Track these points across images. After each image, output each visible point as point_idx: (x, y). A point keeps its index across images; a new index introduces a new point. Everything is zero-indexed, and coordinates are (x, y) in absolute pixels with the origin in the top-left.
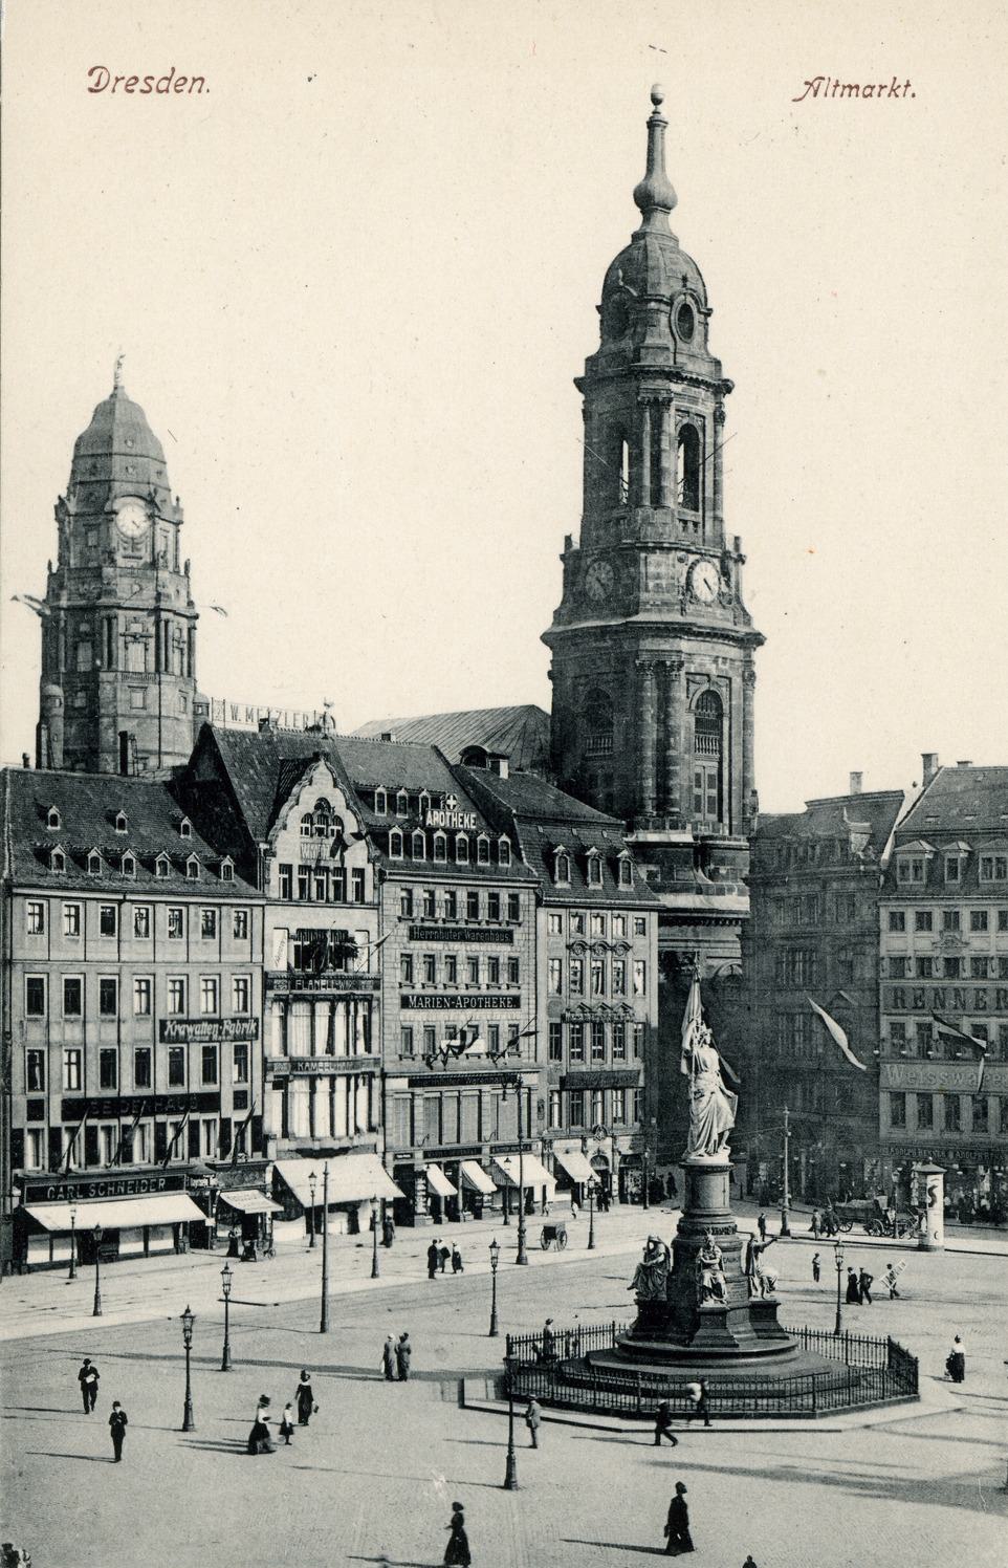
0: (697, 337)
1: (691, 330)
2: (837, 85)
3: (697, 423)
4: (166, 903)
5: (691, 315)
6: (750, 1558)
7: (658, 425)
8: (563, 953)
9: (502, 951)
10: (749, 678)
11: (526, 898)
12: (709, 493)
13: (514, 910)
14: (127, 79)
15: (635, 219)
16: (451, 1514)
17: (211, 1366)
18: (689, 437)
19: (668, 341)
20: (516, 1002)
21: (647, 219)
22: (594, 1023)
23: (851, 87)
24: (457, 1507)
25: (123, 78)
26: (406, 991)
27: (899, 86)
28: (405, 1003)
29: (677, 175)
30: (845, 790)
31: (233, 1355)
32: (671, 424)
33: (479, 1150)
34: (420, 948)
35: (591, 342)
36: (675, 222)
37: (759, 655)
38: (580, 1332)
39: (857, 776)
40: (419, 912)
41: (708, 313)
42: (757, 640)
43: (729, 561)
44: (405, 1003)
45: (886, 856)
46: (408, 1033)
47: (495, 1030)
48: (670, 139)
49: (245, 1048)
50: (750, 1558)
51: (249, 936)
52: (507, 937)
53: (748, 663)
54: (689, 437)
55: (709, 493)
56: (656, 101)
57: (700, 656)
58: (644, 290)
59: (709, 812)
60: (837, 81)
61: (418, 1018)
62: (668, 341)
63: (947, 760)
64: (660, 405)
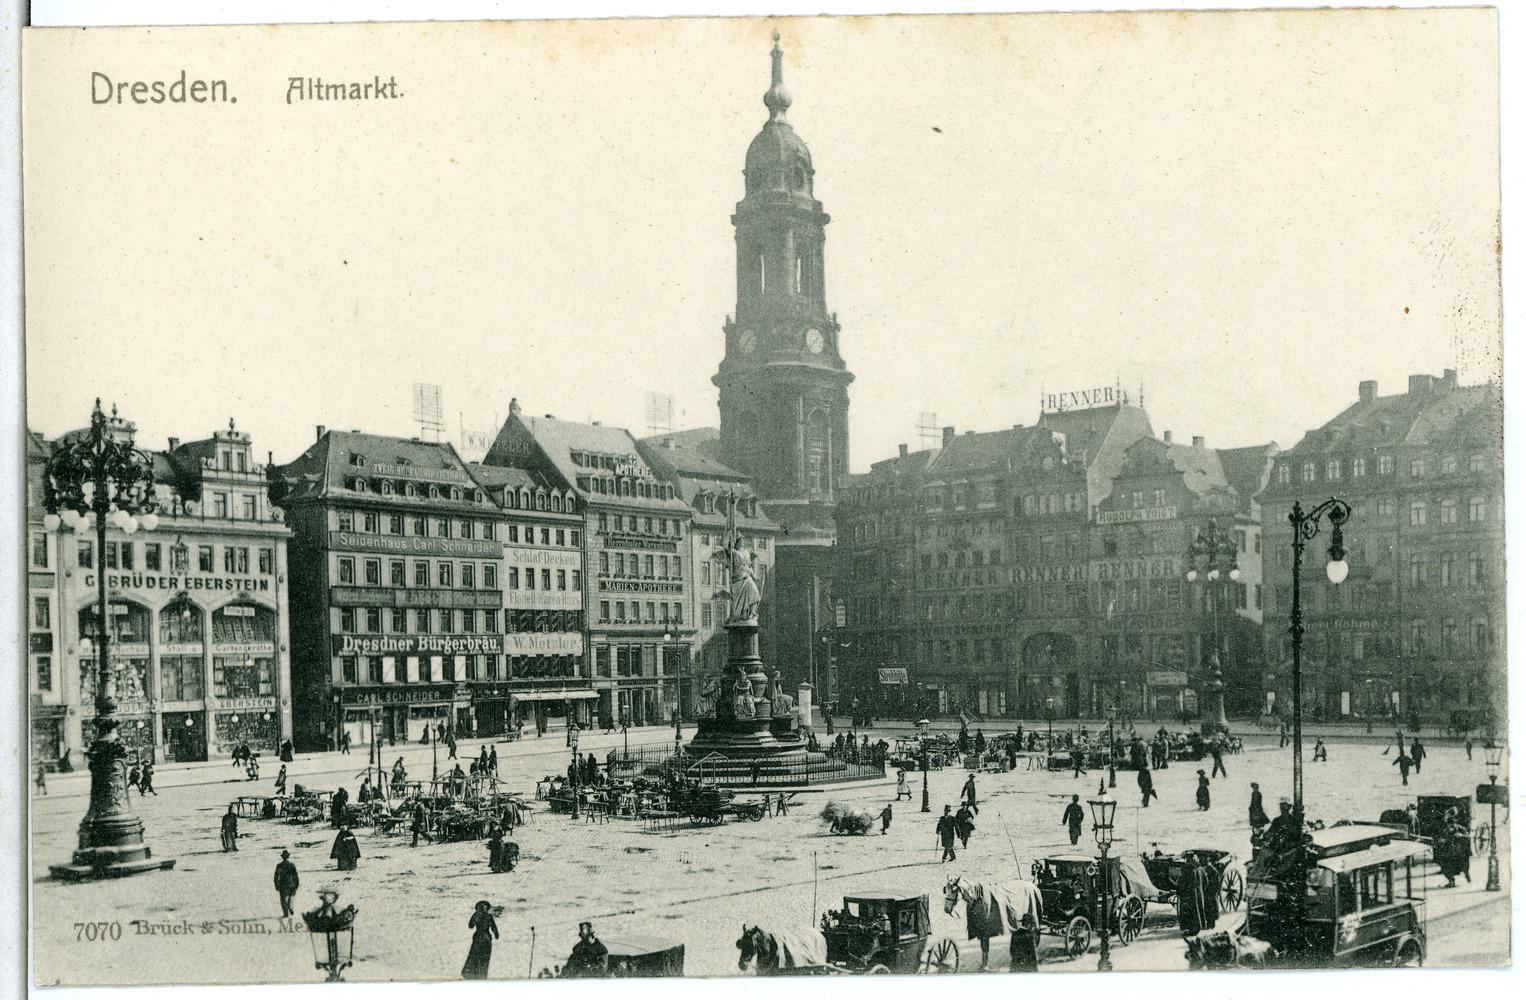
0: (807, 187)
1: (802, 182)
2: (319, 86)
14: (131, 85)
15: (765, 115)
16: (1251, 790)
18: (800, 251)
20: (679, 588)
21: (773, 115)
22: (371, 658)
23: (336, 87)
24: (1255, 786)
25: (126, 84)
26: (603, 579)
27: (385, 86)
28: (603, 586)
29: (789, 87)
35: (740, 193)
36: (790, 117)
43: (830, 329)
46: (605, 604)
47: (665, 605)
49: (369, 580)
51: (273, 570)
59: (129, 578)
60: (319, 80)
63: (959, 431)
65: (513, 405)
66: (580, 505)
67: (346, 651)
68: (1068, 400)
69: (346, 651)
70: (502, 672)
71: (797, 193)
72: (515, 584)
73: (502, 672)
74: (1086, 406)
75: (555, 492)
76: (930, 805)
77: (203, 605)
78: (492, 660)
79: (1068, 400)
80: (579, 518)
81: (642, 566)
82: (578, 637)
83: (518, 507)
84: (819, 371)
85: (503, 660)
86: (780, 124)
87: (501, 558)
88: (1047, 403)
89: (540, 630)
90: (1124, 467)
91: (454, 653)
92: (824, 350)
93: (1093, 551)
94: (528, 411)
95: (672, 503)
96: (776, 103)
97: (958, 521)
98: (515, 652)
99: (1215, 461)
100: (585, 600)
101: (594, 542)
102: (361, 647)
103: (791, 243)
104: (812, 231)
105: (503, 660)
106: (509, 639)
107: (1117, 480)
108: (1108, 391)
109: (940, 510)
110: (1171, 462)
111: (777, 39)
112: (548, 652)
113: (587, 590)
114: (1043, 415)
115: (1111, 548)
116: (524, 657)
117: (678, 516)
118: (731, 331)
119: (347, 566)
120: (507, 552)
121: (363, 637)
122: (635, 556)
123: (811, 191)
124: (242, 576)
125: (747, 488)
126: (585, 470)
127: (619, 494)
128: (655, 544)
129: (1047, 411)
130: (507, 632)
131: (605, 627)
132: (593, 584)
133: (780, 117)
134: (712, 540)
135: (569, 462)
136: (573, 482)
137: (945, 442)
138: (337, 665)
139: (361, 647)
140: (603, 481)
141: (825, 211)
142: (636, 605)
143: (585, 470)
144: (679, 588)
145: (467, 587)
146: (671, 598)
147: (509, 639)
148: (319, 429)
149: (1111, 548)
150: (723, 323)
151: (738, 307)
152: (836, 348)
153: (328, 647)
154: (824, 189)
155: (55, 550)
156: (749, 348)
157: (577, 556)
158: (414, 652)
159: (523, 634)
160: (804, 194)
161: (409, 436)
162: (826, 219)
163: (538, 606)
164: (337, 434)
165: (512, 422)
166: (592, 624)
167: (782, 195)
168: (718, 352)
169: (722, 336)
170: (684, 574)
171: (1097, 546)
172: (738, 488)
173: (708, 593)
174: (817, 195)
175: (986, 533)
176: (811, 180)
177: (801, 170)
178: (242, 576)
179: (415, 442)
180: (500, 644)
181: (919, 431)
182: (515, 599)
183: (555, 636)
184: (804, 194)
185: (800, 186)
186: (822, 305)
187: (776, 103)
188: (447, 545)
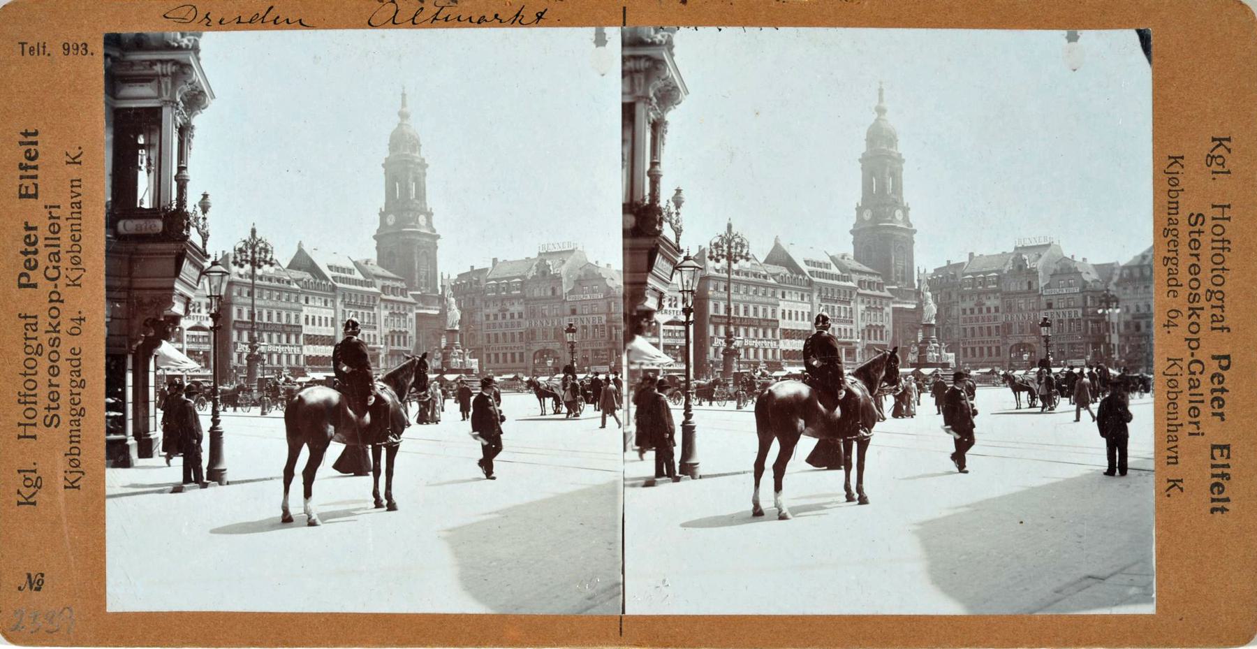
5: (416, 146)
18: (416, 180)
21: (879, 115)
36: (887, 116)
46: (965, 329)
47: (840, 329)
53: (436, 244)
56: (404, 88)
65: (300, 244)
66: (334, 288)
68: (551, 247)
70: (778, 356)
71: (891, 150)
72: (307, 323)
73: (778, 356)
74: (1035, 244)
77: (659, 321)
79: (551, 247)
81: (836, 311)
84: (902, 228)
85: (302, 357)
86: (883, 120)
87: (302, 311)
89: (317, 344)
90: (1055, 270)
91: (282, 353)
92: (427, 224)
93: (1041, 307)
95: (850, 284)
97: (503, 300)
98: (784, 348)
99: (1093, 270)
100: (336, 331)
101: (340, 306)
103: (411, 176)
105: (302, 357)
106: (305, 348)
107: (1052, 276)
108: (1045, 238)
109: (970, 288)
110: (1076, 268)
111: (404, 88)
112: (320, 354)
115: (1050, 306)
116: (310, 356)
117: (852, 289)
118: (859, 210)
120: (781, 303)
121: (761, 340)
122: (369, 314)
124: (199, 315)
125: (880, 279)
126: (336, 274)
128: (843, 302)
129: (541, 251)
133: (882, 117)
134: (866, 300)
136: (808, 274)
137: (970, 260)
141: (426, 162)
142: (845, 330)
143: (336, 274)
144: (375, 328)
147: (305, 348)
148: (700, 246)
149: (574, 312)
150: (379, 211)
151: (862, 199)
152: (431, 223)
153: (708, 343)
154: (424, 153)
159: (787, 340)
160: (417, 155)
162: (427, 166)
163: (317, 333)
165: (300, 251)
167: (407, 156)
169: (378, 217)
170: (377, 321)
171: (568, 311)
172: (874, 279)
173: (864, 325)
175: (992, 298)
177: (892, 140)
178: (675, 309)
180: (301, 349)
182: (307, 329)
183: (323, 347)
184: (417, 155)
185: (892, 147)
187: (881, 111)
188: (765, 300)
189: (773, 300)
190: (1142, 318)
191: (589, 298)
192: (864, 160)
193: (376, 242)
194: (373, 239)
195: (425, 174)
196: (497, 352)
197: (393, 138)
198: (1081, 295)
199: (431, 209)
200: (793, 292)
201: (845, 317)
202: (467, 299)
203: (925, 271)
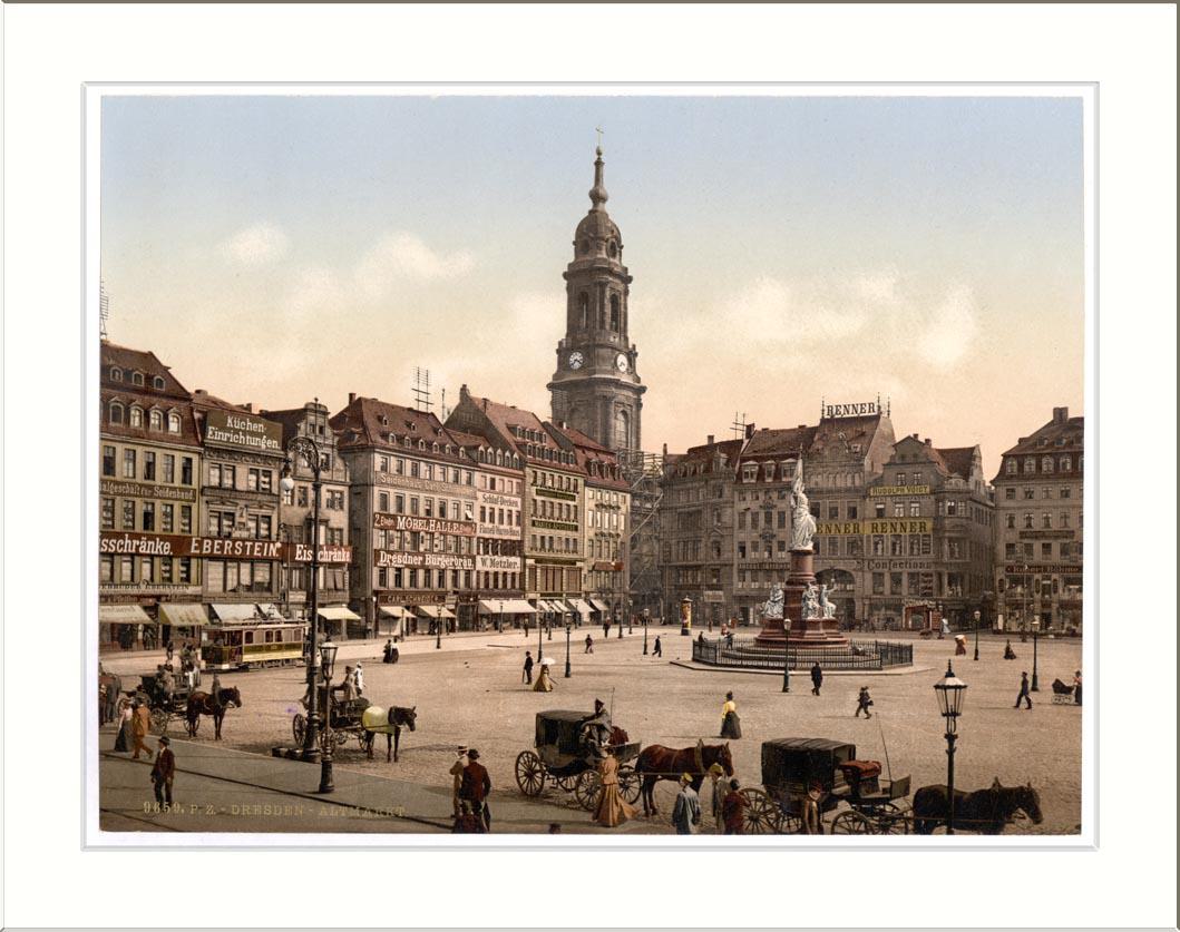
3: (617, 294)
4: (441, 465)
5: (615, 248)
6: (996, 779)
7: (603, 292)
8: (594, 508)
9: (572, 503)
10: (639, 405)
11: (581, 482)
12: (622, 325)
13: (576, 487)
15: (589, 205)
17: (581, 669)
19: (605, 256)
20: (576, 529)
26: (534, 518)
28: (534, 524)
29: (608, 187)
30: (705, 442)
31: (572, 669)
32: (608, 294)
33: (561, 595)
34: (539, 498)
37: (644, 397)
38: (131, 761)
39: (711, 438)
40: (539, 482)
41: (622, 247)
42: (643, 390)
43: (632, 355)
44: (534, 524)
45: (737, 468)
48: (606, 170)
50: (996, 779)
52: (573, 499)
54: (615, 300)
55: (622, 325)
56: (599, 153)
57: (624, 395)
58: (596, 233)
61: (539, 532)
62: (605, 256)
63: (758, 428)
64: (603, 285)
65: (464, 389)
67: (382, 563)
69: (382, 563)
72: (483, 520)
75: (507, 454)
76: (648, 651)
78: (468, 573)
80: (521, 473)
82: (517, 560)
83: (495, 465)
88: (826, 412)
94: (476, 393)
96: (597, 197)
102: (391, 561)
104: (621, 287)
108: (871, 405)
113: (524, 526)
114: (823, 421)
118: (563, 352)
119: (384, 498)
123: (620, 259)
127: (543, 458)
130: (478, 553)
131: (534, 553)
132: (528, 522)
133: (600, 206)
135: (506, 429)
138: (376, 572)
139: (391, 561)
140: (551, 452)
145: (1074, 692)
146: (571, 534)
148: (351, 395)
153: (371, 557)
154: (629, 259)
155: (415, 651)
156: (577, 365)
157: (519, 500)
158: (423, 566)
160: (616, 261)
161: (408, 406)
162: (630, 279)
164: (366, 400)
166: (527, 551)
167: (605, 260)
168: (550, 365)
174: (625, 263)
176: (620, 252)
179: (410, 409)
180: (474, 563)
181: (734, 426)
184: (616, 261)
185: (614, 256)
186: (626, 339)
187: (597, 197)
189: (468, 491)
190: (1057, 537)
191: (906, 491)
192: (571, 275)
193: (550, 394)
194: (546, 390)
195: (626, 292)
196: (898, 570)
197: (580, 231)
198: (933, 497)
199: (634, 346)
200: (506, 479)
201: (560, 518)
202: (710, 488)
203: (665, 451)
